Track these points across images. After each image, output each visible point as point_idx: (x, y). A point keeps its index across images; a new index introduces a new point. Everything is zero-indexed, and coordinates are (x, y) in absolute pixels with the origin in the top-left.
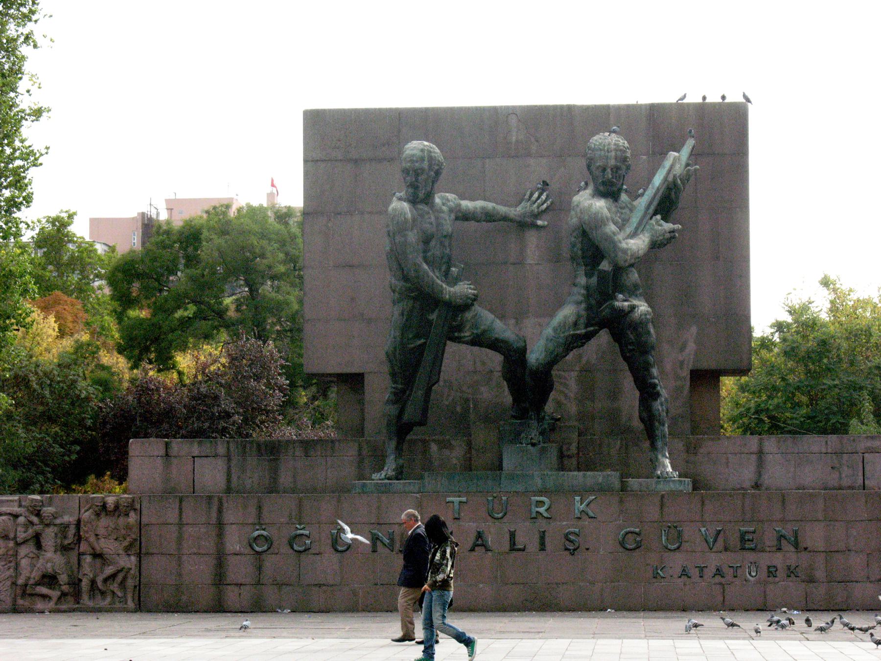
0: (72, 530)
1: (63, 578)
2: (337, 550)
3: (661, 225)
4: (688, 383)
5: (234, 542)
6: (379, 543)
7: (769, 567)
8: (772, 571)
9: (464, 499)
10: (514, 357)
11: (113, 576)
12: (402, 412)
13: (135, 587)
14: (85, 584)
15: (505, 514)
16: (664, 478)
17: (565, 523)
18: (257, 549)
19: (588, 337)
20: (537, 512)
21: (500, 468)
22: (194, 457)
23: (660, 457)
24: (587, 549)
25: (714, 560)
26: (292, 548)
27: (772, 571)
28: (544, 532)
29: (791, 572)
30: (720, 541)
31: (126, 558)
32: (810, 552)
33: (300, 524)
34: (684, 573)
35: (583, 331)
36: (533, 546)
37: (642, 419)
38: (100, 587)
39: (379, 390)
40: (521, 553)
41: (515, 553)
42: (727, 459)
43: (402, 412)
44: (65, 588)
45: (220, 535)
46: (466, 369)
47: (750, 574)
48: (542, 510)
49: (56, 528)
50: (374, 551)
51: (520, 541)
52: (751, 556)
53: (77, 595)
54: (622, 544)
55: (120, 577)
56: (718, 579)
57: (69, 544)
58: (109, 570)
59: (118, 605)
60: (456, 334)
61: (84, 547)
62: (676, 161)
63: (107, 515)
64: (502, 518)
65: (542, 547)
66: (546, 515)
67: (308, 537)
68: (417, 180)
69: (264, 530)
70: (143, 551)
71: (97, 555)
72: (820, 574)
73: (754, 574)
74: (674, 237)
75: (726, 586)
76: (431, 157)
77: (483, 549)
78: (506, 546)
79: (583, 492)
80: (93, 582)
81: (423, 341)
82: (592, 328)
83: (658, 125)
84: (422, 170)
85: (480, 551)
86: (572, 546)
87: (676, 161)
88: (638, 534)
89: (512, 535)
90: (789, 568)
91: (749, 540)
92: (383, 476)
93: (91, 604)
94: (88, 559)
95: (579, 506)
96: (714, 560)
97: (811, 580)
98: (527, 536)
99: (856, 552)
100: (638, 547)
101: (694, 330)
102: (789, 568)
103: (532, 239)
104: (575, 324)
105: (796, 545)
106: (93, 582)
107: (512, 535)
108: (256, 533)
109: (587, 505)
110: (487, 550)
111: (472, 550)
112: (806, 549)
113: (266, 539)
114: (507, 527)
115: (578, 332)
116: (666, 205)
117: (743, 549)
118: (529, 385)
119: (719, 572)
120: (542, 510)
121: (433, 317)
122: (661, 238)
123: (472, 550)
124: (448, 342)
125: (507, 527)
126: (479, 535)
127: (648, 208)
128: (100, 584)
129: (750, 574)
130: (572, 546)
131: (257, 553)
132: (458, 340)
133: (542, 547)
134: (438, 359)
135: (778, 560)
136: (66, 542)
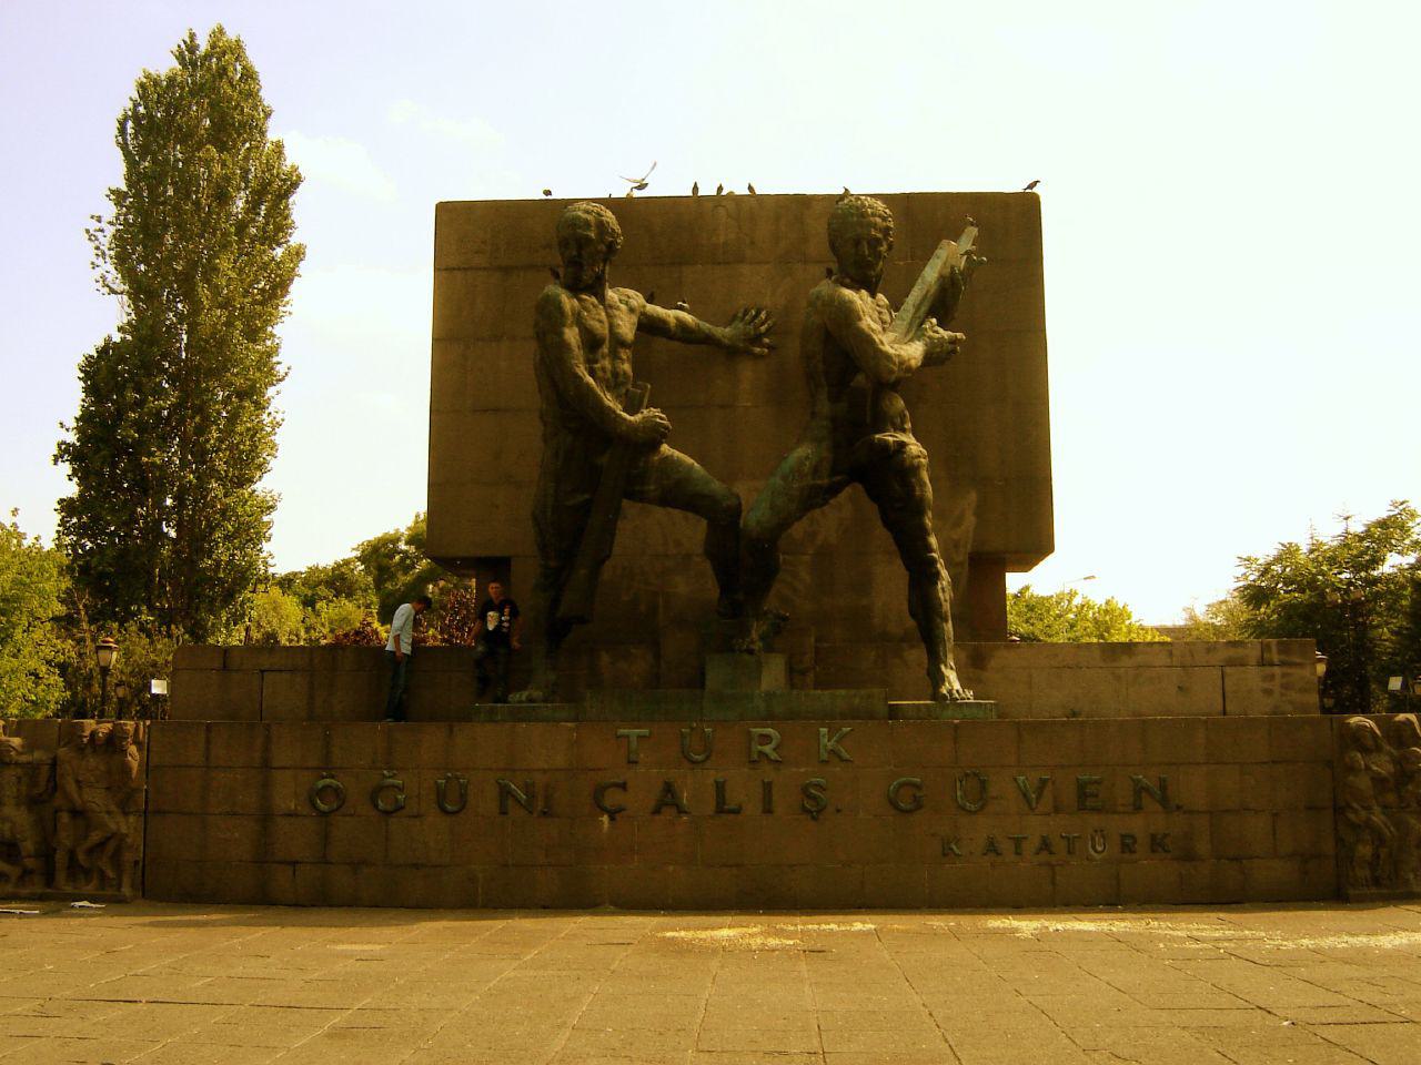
0: (45, 771)
1: (28, 846)
2: (446, 812)
3: (937, 332)
4: (967, 569)
5: (287, 794)
6: (510, 802)
7: (1123, 837)
8: (1128, 844)
9: (645, 731)
10: (723, 520)
11: (102, 845)
12: (555, 602)
13: (136, 863)
14: (60, 858)
15: (708, 758)
16: (951, 701)
17: (802, 770)
18: (323, 807)
19: (834, 490)
20: (761, 753)
21: (702, 685)
22: (262, 671)
23: (943, 667)
24: (838, 811)
25: (1036, 827)
26: (376, 806)
27: (1128, 844)
28: (770, 784)
29: (1157, 844)
30: (1047, 793)
31: (121, 819)
32: (1185, 812)
33: (390, 769)
34: (992, 848)
35: (826, 481)
36: (753, 808)
37: (913, 615)
38: (82, 863)
39: (527, 573)
40: (731, 816)
41: (725, 817)
42: (1030, 676)
43: (555, 602)
44: (30, 863)
45: (266, 785)
46: (656, 546)
47: (1094, 848)
48: (767, 749)
49: (19, 771)
50: (504, 813)
51: (734, 797)
52: (1094, 820)
53: (50, 879)
54: (893, 804)
55: (111, 846)
56: (1044, 857)
57: (41, 795)
58: (95, 837)
59: (110, 892)
60: (638, 488)
61: (58, 801)
62: (952, 254)
63: (94, 752)
64: (703, 761)
65: (768, 810)
66: (774, 756)
67: (401, 789)
68: (580, 255)
69: (333, 777)
70: (150, 808)
71: (77, 813)
72: (1203, 847)
73: (1100, 849)
74: (954, 351)
75: (1057, 868)
76: (602, 222)
77: (674, 811)
78: (711, 808)
79: (826, 717)
80: (72, 854)
81: (586, 496)
82: (839, 478)
83: (927, 216)
84: (588, 239)
85: (668, 813)
86: (813, 806)
87: (952, 254)
88: (918, 787)
89: (720, 788)
90: (1153, 837)
91: (1092, 795)
92: (524, 698)
93: (69, 889)
94: (65, 818)
95: (827, 742)
96: (1036, 827)
97: (1189, 856)
98: (744, 790)
99: (1256, 812)
100: (919, 807)
101: (973, 496)
102: (1153, 837)
103: (747, 372)
104: (816, 471)
105: (1164, 801)
106: (72, 854)
107: (720, 788)
108: (321, 783)
109: (837, 741)
110: (681, 811)
111: (657, 811)
112: (1179, 808)
113: (337, 791)
114: (711, 776)
115: (819, 482)
116: (942, 305)
117: (1082, 808)
118: (743, 562)
119: (1045, 845)
120: (767, 749)
121: (604, 460)
122: (938, 350)
123: (657, 811)
124: (625, 502)
125: (711, 776)
126: (669, 789)
127: (918, 308)
128: (81, 857)
129: (1094, 848)
130: (813, 806)
131: (323, 814)
132: (639, 497)
133: (768, 810)
134: (609, 531)
135: (1136, 825)
136: (35, 791)
